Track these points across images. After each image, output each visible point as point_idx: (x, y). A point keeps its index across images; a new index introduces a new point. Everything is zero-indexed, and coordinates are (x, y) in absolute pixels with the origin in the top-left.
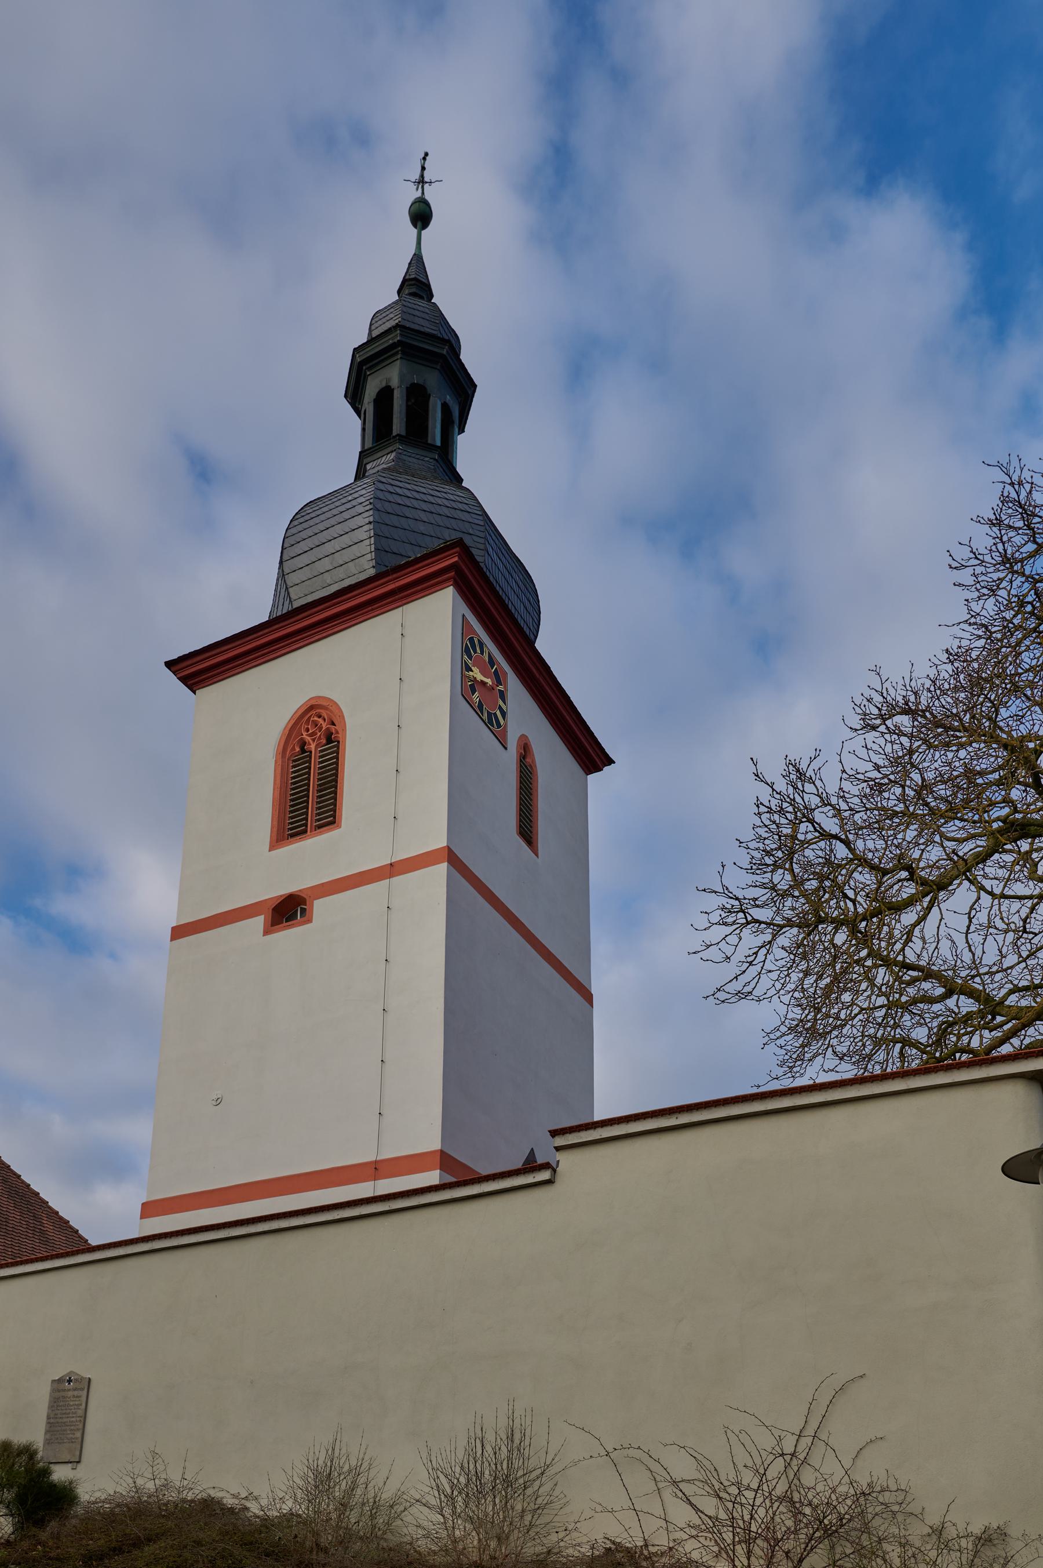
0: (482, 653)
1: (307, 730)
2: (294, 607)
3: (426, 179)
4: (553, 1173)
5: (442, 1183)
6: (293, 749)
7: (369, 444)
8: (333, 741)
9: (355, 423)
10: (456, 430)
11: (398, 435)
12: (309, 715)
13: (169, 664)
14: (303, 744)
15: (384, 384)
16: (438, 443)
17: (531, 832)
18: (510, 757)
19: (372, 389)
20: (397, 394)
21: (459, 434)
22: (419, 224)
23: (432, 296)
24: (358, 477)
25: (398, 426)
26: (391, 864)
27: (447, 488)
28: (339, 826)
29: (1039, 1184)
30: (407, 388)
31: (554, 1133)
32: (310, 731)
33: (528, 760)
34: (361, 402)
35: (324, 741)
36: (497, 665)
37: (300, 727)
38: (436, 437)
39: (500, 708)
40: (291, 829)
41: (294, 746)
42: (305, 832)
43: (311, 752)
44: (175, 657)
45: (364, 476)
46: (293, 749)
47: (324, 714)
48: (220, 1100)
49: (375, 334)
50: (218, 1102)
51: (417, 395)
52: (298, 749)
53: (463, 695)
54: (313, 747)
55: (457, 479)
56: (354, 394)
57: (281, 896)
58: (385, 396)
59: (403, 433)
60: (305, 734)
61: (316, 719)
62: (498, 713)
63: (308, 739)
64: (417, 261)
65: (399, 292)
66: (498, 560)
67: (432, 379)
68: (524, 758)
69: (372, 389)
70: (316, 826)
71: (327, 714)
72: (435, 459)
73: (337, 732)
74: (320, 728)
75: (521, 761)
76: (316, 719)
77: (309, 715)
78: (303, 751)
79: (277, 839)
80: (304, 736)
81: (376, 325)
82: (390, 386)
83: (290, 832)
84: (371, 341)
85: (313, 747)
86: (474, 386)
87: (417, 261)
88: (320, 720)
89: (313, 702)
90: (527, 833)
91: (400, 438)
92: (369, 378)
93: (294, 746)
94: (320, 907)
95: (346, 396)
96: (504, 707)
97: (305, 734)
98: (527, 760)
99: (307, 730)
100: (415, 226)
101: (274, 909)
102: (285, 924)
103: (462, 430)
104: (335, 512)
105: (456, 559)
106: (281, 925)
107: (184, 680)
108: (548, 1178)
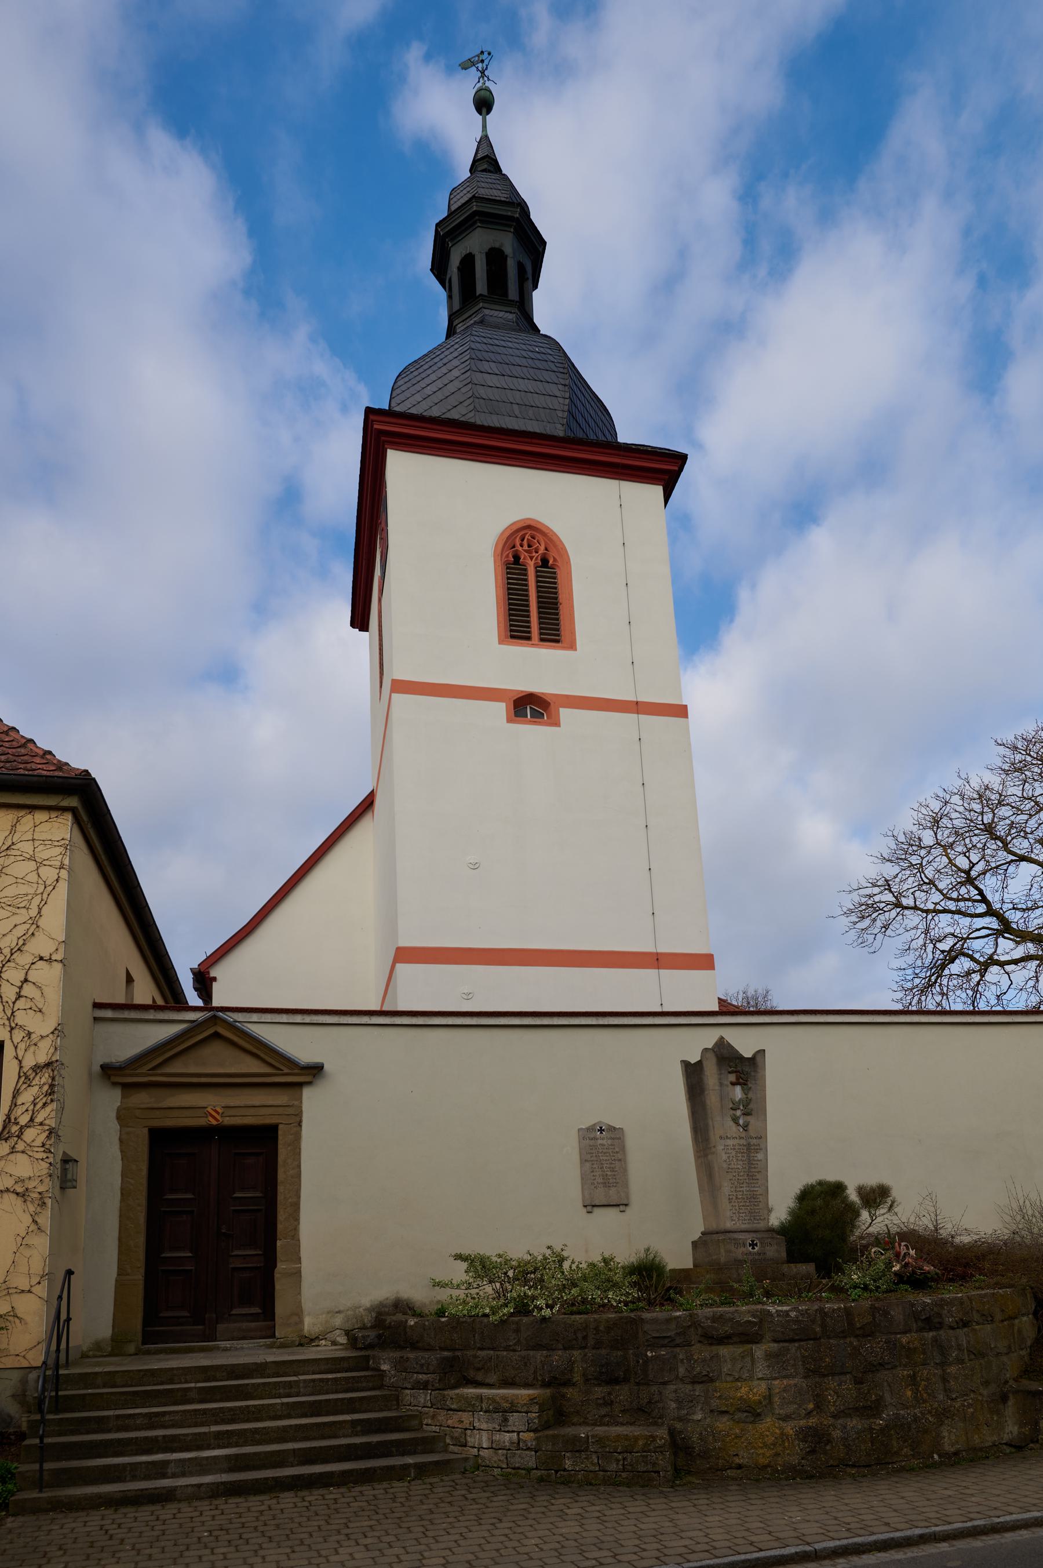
7: (456, 306)
9: (441, 293)
19: (455, 260)
21: (534, 290)
22: (484, 111)
24: (448, 336)
27: (534, 334)
31: (97, 1006)
34: (445, 273)
38: (513, 293)
45: (455, 333)
48: (477, 865)
49: (453, 208)
50: (475, 867)
51: (496, 257)
55: (536, 329)
56: (439, 268)
58: (468, 261)
64: (485, 141)
66: (578, 401)
69: (455, 260)
81: (455, 199)
84: (451, 214)
86: (544, 243)
87: (485, 141)
92: (452, 249)
95: (432, 270)
100: (480, 113)
103: (535, 286)
104: (423, 375)
106: (516, 698)
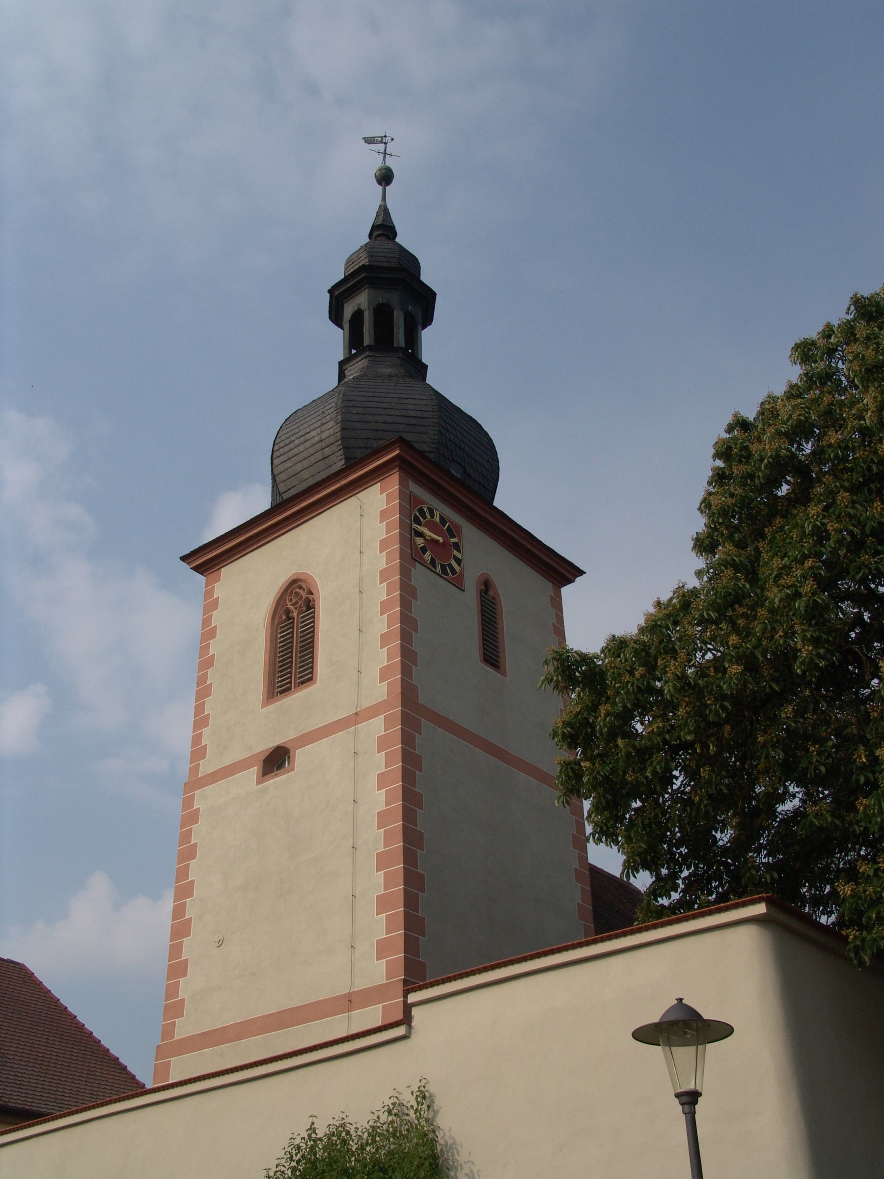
0: (432, 515)
1: (291, 600)
2: (284, 499)
3: (382, 156)
4: (408, 1027)
5: (383, 1024)
6: (281, 617)
8: (310, 606)
10: (420, 328)
11: (367, 346)
12: (292, 588)
13: (184, 558)
14: (288, 612)
15: (356, 308)
16: (402, 344)
17: (497, 657)
18: (470, 598)
19: (349, 310)
20: (367, 315)
21: (422, 330)
23: (395, 234)
25: (367, 340)
26: (356, 713)
28: (315, 682)
29: (660, 1045)
30: (374, 309)
32: (293, 601)
33: (491, 593)
35: (305, 609)
36: (450, 521)
37: (286, 599)
38: (400, 338)
39: (456, 558)
40: (280, 687)
41: (281, 615)
42: (289, 689)
43: (294, 619)
44: (188, 552)
46: (281, 617)
47: (304, 586)
51: (382, 314)
52: (284, 617)
53: (413, 558)
54: (295, 615)
56: (336, 316)
57: (270, 748)
58: (358, 315)
59: (372, 343)
60: (289, 603)
61: (298, 590)
62: (453, 563)
63: (292, 608)
64: (384, 211)
65: (370, 235)
67: (394, 298)
68: (486, 592)
69: (349, 310)
70: (299, 683)
71: (306, 586)
72: (400, 357)
73: (314, 600)
74: (302, 597)
75: (481, 596)
76: (298, 590)
77: (292, 588)
78: (289, 618)
79: (267, 697)
80: (289, 606)
82: (361, 310)
83: (301, 680)
85: (295, 615)
87: (384, 211)
88: (301, 591)
89: (295, 578)
90: (493, 659)
91: (369, 347)
93: (281, 615)
94: (301, 757)
96: (459, 556)
97: (289, 603)
98: (489, 593)
99: (291, 600)
101: (264, 761)
102: (276, 773)
105: (398, 452)
107: (196, 569)
108: (403, 1034)
